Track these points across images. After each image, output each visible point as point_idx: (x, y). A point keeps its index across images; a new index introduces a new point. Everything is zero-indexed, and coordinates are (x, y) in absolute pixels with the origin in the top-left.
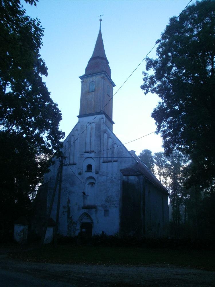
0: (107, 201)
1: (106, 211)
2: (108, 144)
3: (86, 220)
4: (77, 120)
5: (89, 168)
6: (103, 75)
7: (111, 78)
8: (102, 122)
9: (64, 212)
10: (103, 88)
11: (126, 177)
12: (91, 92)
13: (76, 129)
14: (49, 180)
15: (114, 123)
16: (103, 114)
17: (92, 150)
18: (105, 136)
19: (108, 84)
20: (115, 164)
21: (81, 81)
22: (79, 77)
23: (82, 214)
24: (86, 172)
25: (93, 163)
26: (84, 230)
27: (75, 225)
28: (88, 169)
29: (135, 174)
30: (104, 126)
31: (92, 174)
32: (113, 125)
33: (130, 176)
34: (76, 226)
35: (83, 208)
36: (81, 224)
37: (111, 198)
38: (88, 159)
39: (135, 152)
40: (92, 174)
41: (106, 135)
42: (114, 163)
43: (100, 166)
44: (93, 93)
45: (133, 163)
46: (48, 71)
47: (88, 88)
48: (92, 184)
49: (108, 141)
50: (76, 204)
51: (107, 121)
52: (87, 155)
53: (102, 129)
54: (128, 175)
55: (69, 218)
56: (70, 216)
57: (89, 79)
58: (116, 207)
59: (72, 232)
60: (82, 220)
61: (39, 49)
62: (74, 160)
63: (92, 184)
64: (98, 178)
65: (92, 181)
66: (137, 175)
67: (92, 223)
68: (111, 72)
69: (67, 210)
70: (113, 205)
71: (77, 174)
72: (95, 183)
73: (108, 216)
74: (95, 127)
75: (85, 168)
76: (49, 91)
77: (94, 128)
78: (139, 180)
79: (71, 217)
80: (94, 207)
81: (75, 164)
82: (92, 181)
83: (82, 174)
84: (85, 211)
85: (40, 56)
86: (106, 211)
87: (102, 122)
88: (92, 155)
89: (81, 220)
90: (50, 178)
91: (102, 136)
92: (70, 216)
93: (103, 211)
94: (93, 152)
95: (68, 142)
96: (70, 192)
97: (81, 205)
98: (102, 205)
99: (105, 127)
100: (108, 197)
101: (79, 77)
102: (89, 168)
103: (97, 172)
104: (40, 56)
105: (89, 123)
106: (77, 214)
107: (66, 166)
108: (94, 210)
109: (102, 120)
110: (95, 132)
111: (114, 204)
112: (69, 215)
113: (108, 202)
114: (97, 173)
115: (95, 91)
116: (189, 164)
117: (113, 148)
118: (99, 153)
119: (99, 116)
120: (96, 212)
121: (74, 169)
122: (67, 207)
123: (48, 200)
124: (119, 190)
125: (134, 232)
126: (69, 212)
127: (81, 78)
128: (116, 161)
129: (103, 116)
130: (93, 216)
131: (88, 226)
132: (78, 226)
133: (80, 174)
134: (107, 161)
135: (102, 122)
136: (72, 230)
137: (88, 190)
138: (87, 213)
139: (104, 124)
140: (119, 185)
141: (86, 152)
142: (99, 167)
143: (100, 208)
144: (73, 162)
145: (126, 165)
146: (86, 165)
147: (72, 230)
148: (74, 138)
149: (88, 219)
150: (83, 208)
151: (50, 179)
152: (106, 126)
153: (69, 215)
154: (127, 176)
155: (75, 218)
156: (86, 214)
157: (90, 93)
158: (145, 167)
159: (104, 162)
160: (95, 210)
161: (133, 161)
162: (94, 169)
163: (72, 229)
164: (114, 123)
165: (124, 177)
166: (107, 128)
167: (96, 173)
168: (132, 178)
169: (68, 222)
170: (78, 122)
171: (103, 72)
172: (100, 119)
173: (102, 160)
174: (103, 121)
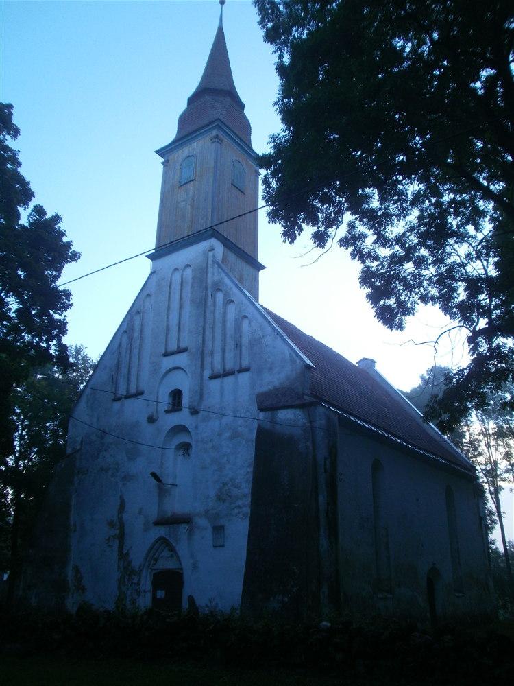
0: (220, 498)
1: (218, 530)
2: (224, 322)
3: (166, 563)
4: (146, 266)
5: (177, 395)
6: (214, 133)
7: (251, 148)
8: (210, 259)
9: (109, 539)
10: (216, 167)
11: (268, 414)
12: (186, 183)
13: (145, 293)
14: (78, 447)
15: (262, 267)
16: (212, 236)
17: (183, 345)
18: (217, 300)
19: (234, 158)
20: (244, 378)
21: (162, 160)
22: (157, 152)
24: (167, 412)
25: (184, 383)
26: (161, 594)
28: (174, 405)
29: (298, 402)
30: (216, 270)
31: (183, 417)
32: (261, 273)
33: (279, 411)
34: (139, 580)
35: (157, 524)
36: (155, 574)
38: (171, 374)
39: (373, 362)
40: (183, 417)
41: (220, 296)
42: (240, 375)
43: (201, 389)
44: (190, 186)
45: (292, 371)
46: (16, 120)
47: (177, 177)
48: (185, 448)
49: (225, 313)
50: (140, 513)
51: (232, 257)
52: (168, 363)
53: (210, 282)
54: (274, 409)
55: (123, 556)
56: (125, 552)
57: (180, 152)
60: (156, 560)
61: (431, 302)
62: (138, 382)
63: (185, 448)
64: (196, 427)
65: (182, 438)
66: (303, 406)
67: (182, 569)
68: (248, 123)
69: (117, 532)
70: (236, 511)
71: (143, 421)
73: (223, 546)
74: (193, 278)
75: (165, 399)
76: (27, 180)
77: (190, 281)
78: (311, 422)
79: (128, 554)
80: (186, 520)
81: (139, 393)
82: (182, 438)
83: (156, 420)
84: (162, 531)
86: (218, 530)
87: (210, 259)
88: (182, 360)
89: (153, 562)
90: (80, 442)
91: (210, 300)
92: (125, 552)
93: (210, 530)
94: (185, 350)
95: (125, 332)
96: (127, 478)
97: (153, 514)
99: (219, 272)
100: (224, 484)
101: (157, 152)
102: (177, 395)
105: (176, 269)
106: (141, 542)
107: (120, 401)
108: (184, 528)
109: (211, 254)
110: (192, 293)
111: (239, 507)
112: (121, 547)
114: (194, 412)
115: (193, 180)
117: (238, 328)
118: (202, 355)
119: (203, 246)
120: (191, 532)
121: (135, 410)
122: (118, 524)
123: (73, 503)
125: (286, 599)
126: (121, 537)
127: (161, 152)
128: (247, 370)
129: (213, 242)
130: (182, 549)
131: (171, 581)
132: (146, 584)
133: (151, 420)
134: (221, 372)
135: (210, 262)
137: (177, 469)
138: (167, 537)
139: (216, 266)
141: (167, 354)
142: (200, 393)
143: (202, 522)
144: (137, 387)
145: (272, 380)
146: (169, 392)
147: (129, 593)
148: (142, 319)
150: (157, 524)
151: (82, 442)
152: (220, 270)
153: (121, 547)
154: (270, 413)
155: (137, 557)
156: (163, 541)
157: (182, 188)
158: (413, 413)
159: (212, 378)
161: (293, 362)
162: (186, 401)
164: (262, 267)
165: (262, 415)
166: (223, 275)
168: (285, 415)
170: (152, 273)
171: (213, 122)
172: (206, 253)
173: (207, 373)
174: (214, 256)
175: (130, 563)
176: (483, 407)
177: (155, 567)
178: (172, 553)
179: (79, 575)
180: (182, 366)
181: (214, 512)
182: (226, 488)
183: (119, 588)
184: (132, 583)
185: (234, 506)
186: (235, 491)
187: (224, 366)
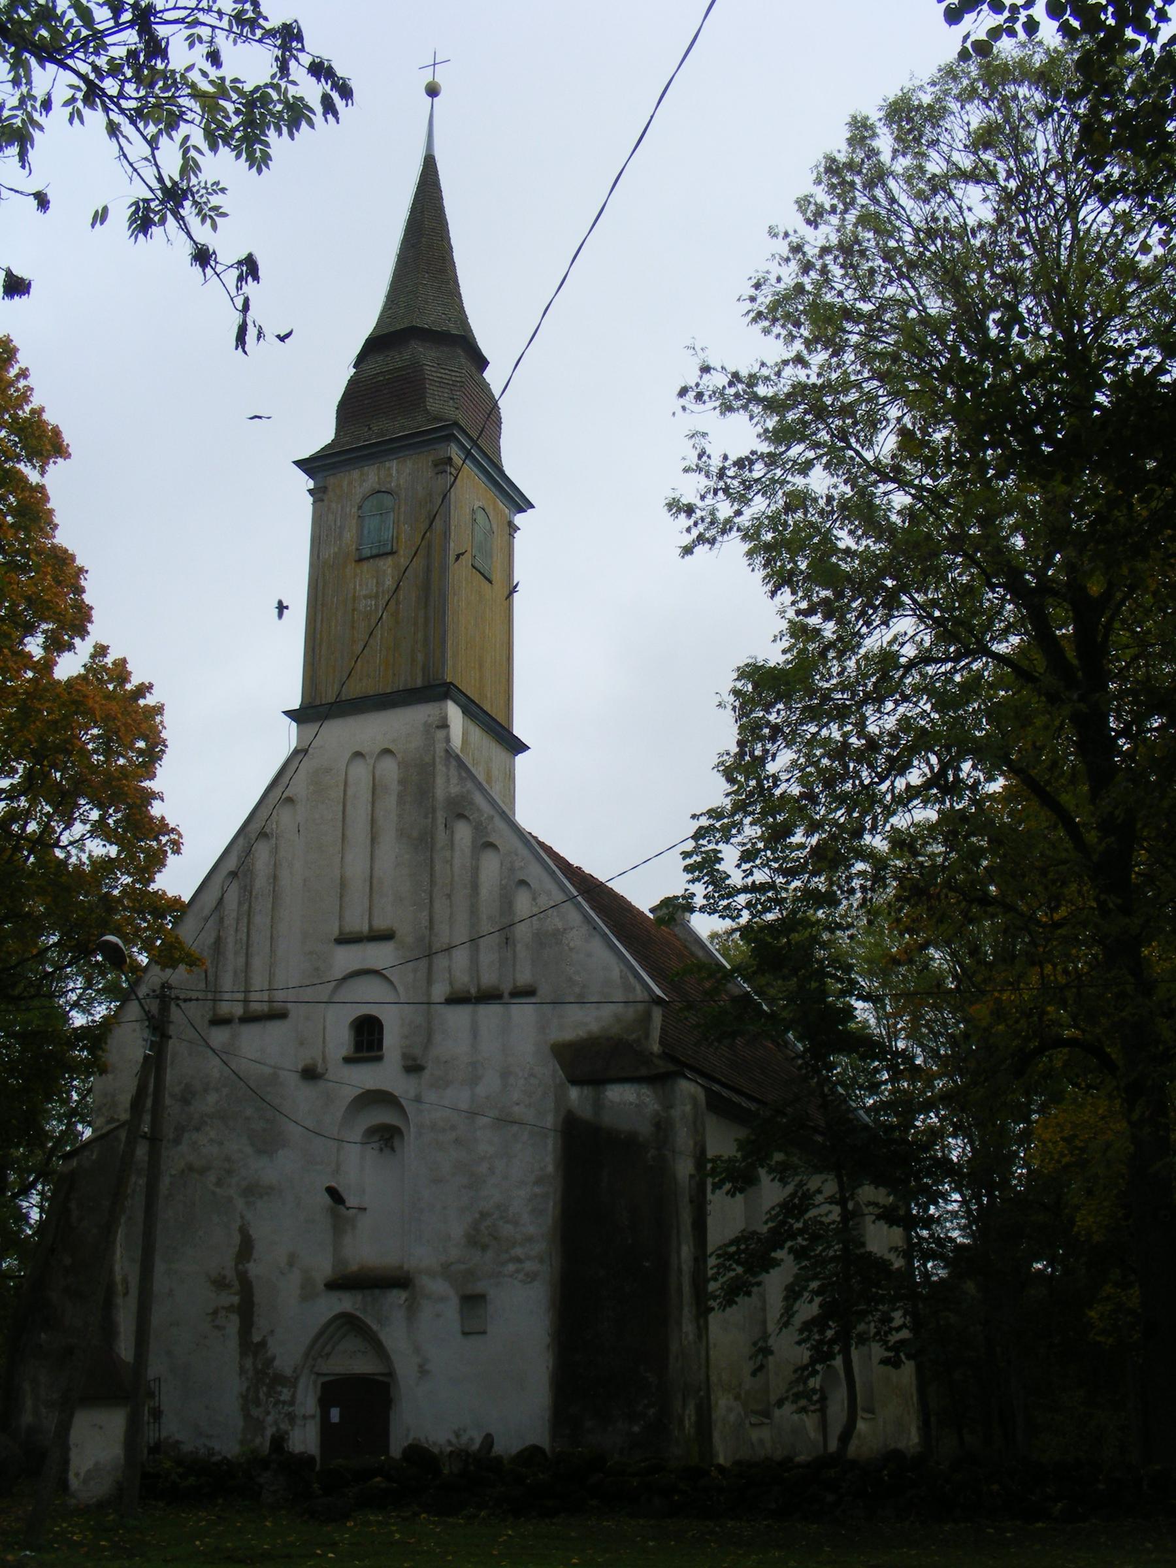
0: (474, 1240)
58: (531, 1277)
70: (511, 1267)
79: (263, 1344)
84: (346, 1303)
100: (484, 1215)
108: (398, 1297)
163: (268, 1413)
169: (242, 1371)
181: (462, 1267)
186: (507, 1230)
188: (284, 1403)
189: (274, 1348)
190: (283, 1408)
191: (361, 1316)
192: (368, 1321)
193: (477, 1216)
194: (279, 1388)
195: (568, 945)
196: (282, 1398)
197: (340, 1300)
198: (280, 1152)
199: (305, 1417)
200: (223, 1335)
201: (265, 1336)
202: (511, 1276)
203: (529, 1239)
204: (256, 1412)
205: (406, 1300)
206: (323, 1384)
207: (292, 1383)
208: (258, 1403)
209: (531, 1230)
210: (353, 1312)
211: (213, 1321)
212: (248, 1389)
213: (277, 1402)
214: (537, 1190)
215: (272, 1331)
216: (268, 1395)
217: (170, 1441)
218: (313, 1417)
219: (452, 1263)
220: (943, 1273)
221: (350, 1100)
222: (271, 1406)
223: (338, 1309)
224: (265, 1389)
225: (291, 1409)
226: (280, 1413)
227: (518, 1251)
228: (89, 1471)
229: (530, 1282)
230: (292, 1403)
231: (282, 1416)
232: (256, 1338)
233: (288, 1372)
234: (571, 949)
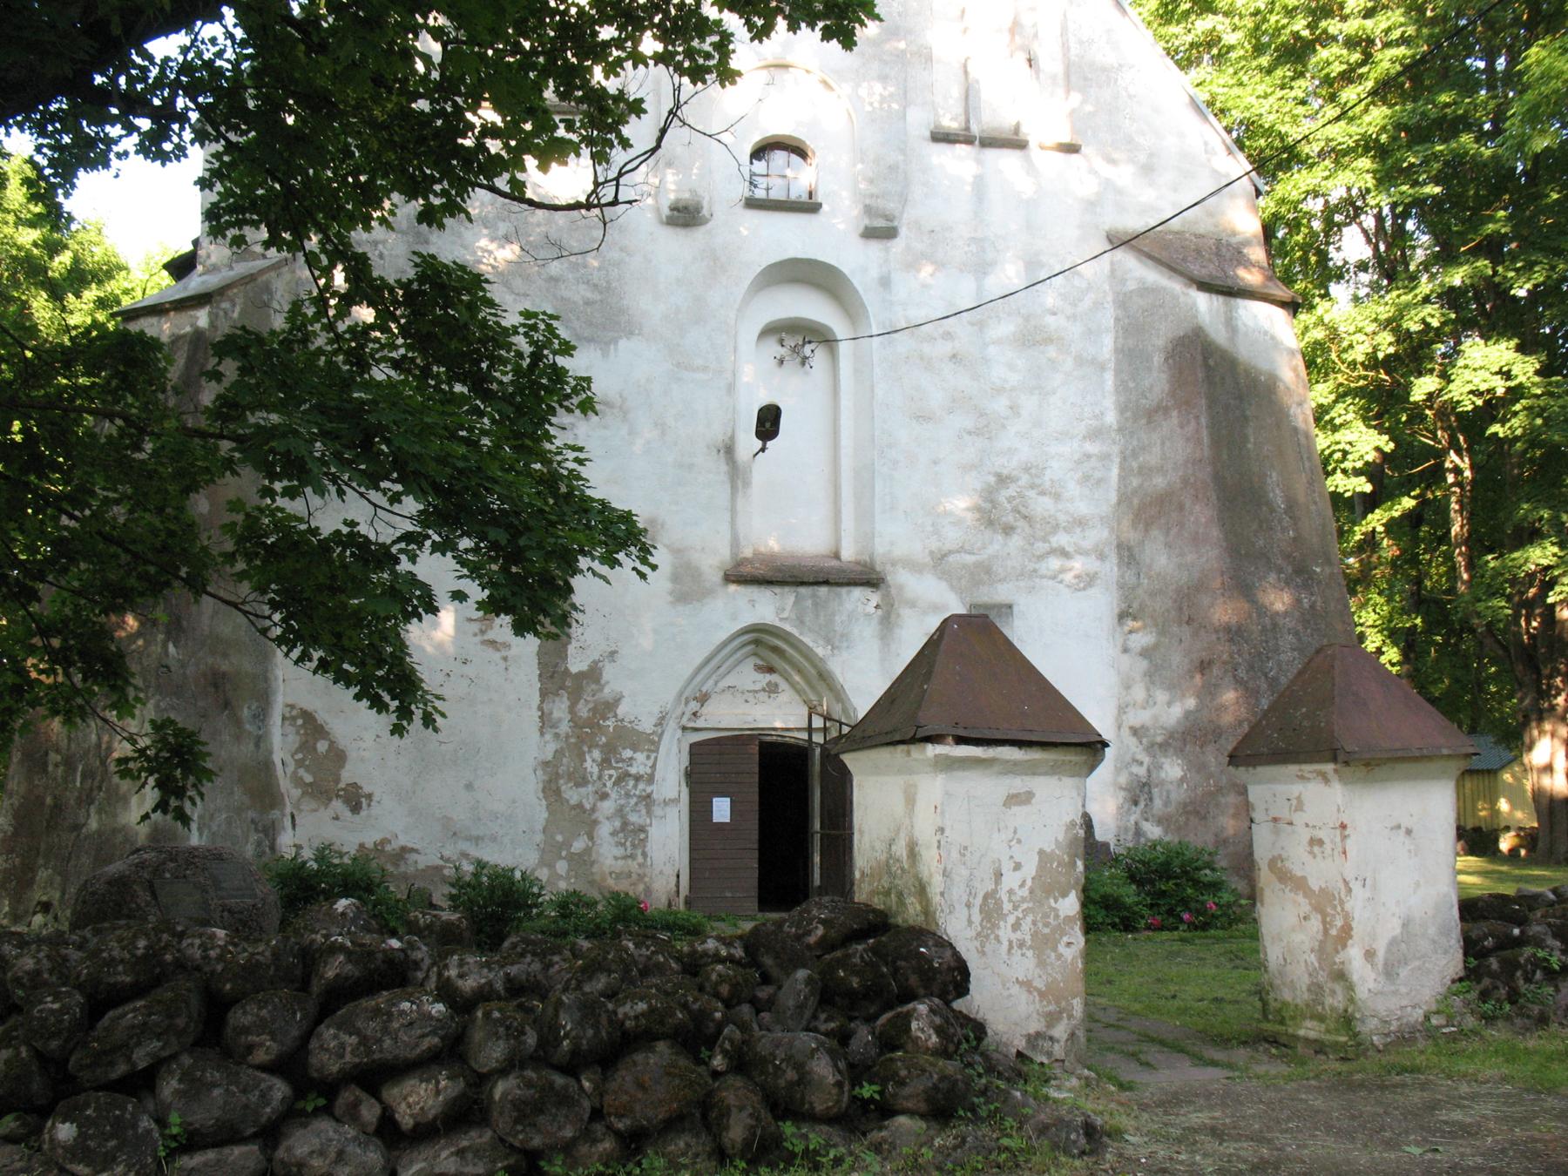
0: (990, 517)
23: (725, 644)
27: (640, 763)
37: (1032, 494)
38: (654, 144)
58: (1088, 581)
59: (604, 830)
60: (703, 699)
64: (885, 282)
70: (1055, 563)
72: (839, 328)
79: (593, 674)
84: (766, 607)
85: (793, 27)
89: (694, 706)
98: (939, 562)
100: (1003, 480)
103: (889, 218)
104: (793, 27)
108: (859, 600)
111: (1064, 554)
113: (1008, 530)
116: (1101, 603)
124: (1111, 418)
136: (607, 807)
138: (788, 627)
140: (1109, 379)
149: (772, 689)
159: (942, 137)
160: (875, 598)
163: (604, 796)
167: (870, 234)
169: (546, 721)
175: (608, 707)
176: (351, 534)
177: (700, 723)
178: (768, 677)
179: (322, 746)
180: (660, 151)
181: (969, 559)
182: (1011, 491)
183: (551, 791)
184: (627, 775)
185: (1041, 547)
186: (1042, 506)
187: (968, 121)
188: (638, 778)
189: (614, 680)
190: (635, 787)
191: (795, 632)
192: (807, 640)
193: (992, 479)
194: (627, 753)
195: (1126, 89)
196: (633, 770)
197: (752, 602)
198: (623, 343)
199: (666, 803)
200: (505, 659)
201: (596, 663)
202: (1054, 578)
203: (1081, 523)
204: (572, 795)
205: (877, 607)
206: (692, 746)
207: (650, 744)
208: (582, 781)
209: (1083, 508)
210: (778, 624)
211: (482, 632)
212: (558, 753)
213: (623, 778)
214: (1092, 448)
215: (613, 653)
216: (605, 763)
217: (388, 848)
218: (676, 801)
219: (950, 552)
220: (18, 438)
221: (759, 270)
222: (609, 784)
223: (748, 619)
224: (597, 754)
225: (649, 790)
226: (628, 795)
227: (1061, 540)
228: (1393, 942)
229: (1084, 589)
230: (651, 779)
231: (633, 801)
232: (577, 663)
233: (647, 726)
234: (1130, 97)
